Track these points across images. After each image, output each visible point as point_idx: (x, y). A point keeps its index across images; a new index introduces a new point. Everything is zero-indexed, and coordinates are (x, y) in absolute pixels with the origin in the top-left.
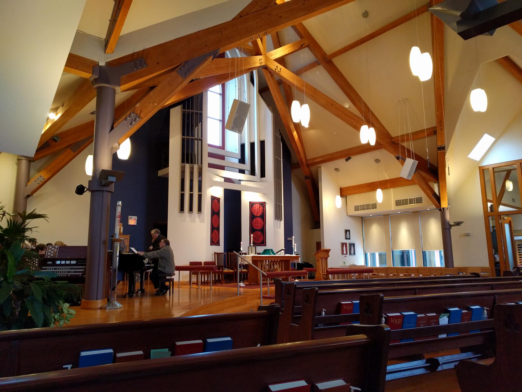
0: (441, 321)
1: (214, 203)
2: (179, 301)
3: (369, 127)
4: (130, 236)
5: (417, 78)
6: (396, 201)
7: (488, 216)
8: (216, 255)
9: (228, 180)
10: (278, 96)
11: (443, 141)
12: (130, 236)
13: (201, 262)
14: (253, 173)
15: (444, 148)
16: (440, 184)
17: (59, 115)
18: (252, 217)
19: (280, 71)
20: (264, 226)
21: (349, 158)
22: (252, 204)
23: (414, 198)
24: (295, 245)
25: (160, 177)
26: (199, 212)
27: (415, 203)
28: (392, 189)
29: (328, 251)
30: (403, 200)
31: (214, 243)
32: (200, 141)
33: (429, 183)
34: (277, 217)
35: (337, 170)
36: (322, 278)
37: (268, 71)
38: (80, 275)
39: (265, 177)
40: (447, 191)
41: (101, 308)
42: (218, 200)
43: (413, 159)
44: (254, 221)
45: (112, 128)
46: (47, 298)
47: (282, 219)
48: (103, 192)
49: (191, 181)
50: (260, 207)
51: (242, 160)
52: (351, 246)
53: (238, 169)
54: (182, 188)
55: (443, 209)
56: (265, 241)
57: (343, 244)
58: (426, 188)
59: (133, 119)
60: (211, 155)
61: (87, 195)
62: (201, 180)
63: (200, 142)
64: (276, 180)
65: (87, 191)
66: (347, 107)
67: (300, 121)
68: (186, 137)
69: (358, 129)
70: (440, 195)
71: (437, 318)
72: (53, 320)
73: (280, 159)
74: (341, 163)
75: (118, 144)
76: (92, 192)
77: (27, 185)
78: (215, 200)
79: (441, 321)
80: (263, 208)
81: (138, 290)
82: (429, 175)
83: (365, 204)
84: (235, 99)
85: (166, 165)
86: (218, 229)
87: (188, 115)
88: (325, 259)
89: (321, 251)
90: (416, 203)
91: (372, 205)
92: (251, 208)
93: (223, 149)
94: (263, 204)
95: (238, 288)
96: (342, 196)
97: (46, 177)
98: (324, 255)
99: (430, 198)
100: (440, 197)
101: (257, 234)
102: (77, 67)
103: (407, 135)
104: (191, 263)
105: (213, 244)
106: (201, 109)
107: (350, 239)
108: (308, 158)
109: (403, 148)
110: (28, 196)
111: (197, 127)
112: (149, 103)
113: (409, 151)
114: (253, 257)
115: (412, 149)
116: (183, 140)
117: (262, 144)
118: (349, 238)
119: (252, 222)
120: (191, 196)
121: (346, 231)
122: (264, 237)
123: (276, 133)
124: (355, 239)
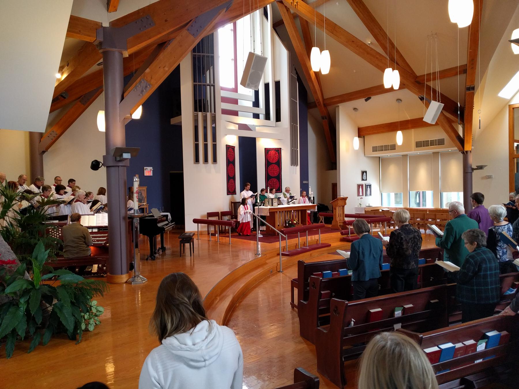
0: (479, 348)
1: (229, 151)
2: (199, 252)
3: (393, 70)
4: (147, 187)
5: (455, 25)
6: (416, 142)
7: (514, 158)
8: (233, 204)
9: (243, 127)
10: (294, 32)
11: (473, 81)
12: (147, 187)
13: (218, 212)
14: (267, 117)
15: (473, 88)
16: (465, 127)
17: (65, 76)
18: (268, 164)
19: (296, 5)
20: (279, 173)
21: (369, 98)
22: (267, 151)
23: (436, 140)
24: (312, 193)
25: (172, 125)
26: (215, 163)
27: (436, 145)
28: (413, 129)
29: (345, 199)
30: (423, 141)
31: (230, 192)
32: (213, 87)
33: (452, 124)
34: (293, 162)
35: (355, 110)
36: (339, 226)
37: (283, 5)
38: (103, 244)
39: (280, 121)
40: (472, 134)
41: (126, 282)
42: (233, 148)
43: (439, 101)
44: (269, 168)
45: (122, 98)
46: (75, 301)
47: (298, 165)
48: (118, 168)
49: (205, 128)
50: (275, 153)
51: (256, 104)
52: (367, 188)
53: (252, 113)
54: (196, 138)
55: (467, 152)
56: (281, 188)
57: (359, 186)
58: (450, 130)
59: (144, 87)
60: (225, 100)
61: (103, 170)
62: (215, 126)
63: (212, 87)
64: (292, 124)
65: (103, 166)
66: (369, 43)
67: (320, 70)
68: (197, 83)
69: (383, 71)
70: (464, 138)
71: (475, 346)
72: (84, 320)
73: (295, 101)
74: (360, 103)
75: (130, 115)
76: (108, 167)
77: (41, 141)
78: (230, 149)
79: (479, 348)
80: (279, 154)
81: (159, 248)
82: (454, 116)
83: (383, 145)
84: (250, 51)
85: (179, 113)
86: (234, 178)
87: (199, 58)
88: (342, 207)
89: (338, 199)
90: (438, 145)
91: (391, 146)
92: (266, 155)
93: (236, 92)
94: (279, 150)
95: (257, 241)
96: (359, 136)
97: (58, 132)
98: (340, 203)
99: (453, 140)
100: (464, 139)
101: (273, 181)
102: (80, 31)
103: (434, 73)
104: (210, 215)
105: (229, 194)
106: (213, 53)
107: (366, 180)
108: (325, 97)
109: (429, 88)
110: (44, 152)
111: (208, 71)
112: (160, 67)
113: (434, 91)
114: (270, 209)
115: (438, 89)
116: (195, 87)
117: (277, 85)
118: (365, 179)
119: (267, 169)
120: (206, 146)
121: (363, 172)
122: (280, 183)
123: (291, 73)
124: (372, 180)
